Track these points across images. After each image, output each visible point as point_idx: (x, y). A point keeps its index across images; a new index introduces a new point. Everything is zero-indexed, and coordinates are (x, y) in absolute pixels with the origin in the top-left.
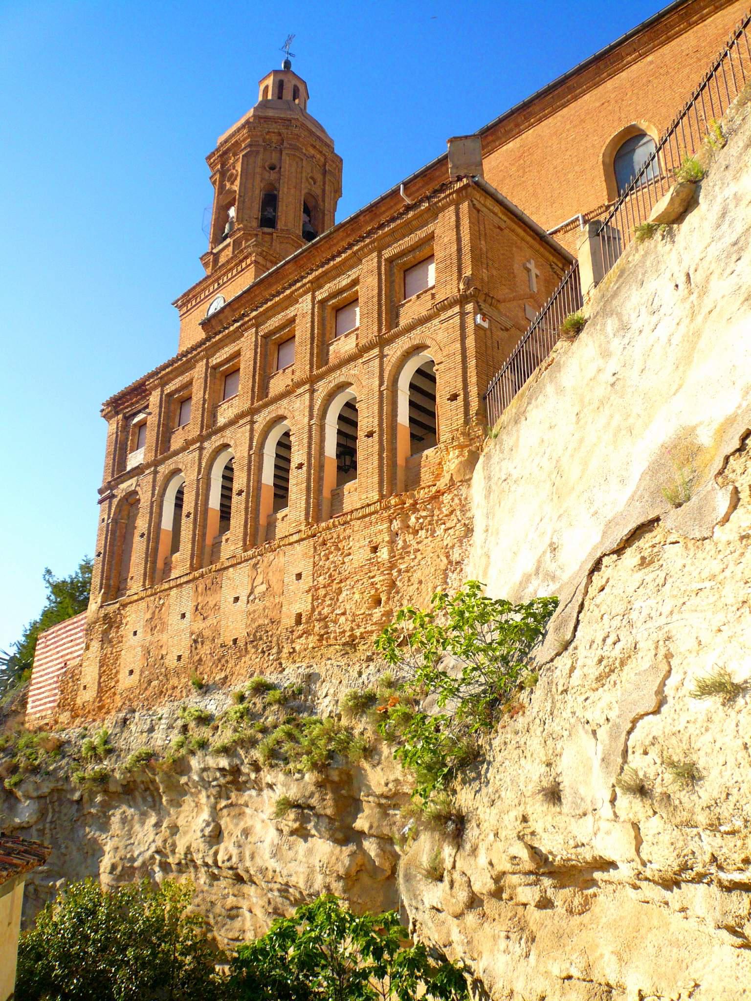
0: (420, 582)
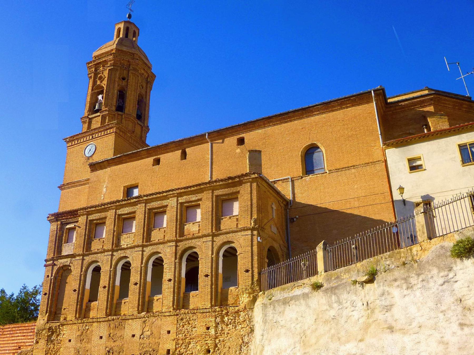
0: (230, 348)
